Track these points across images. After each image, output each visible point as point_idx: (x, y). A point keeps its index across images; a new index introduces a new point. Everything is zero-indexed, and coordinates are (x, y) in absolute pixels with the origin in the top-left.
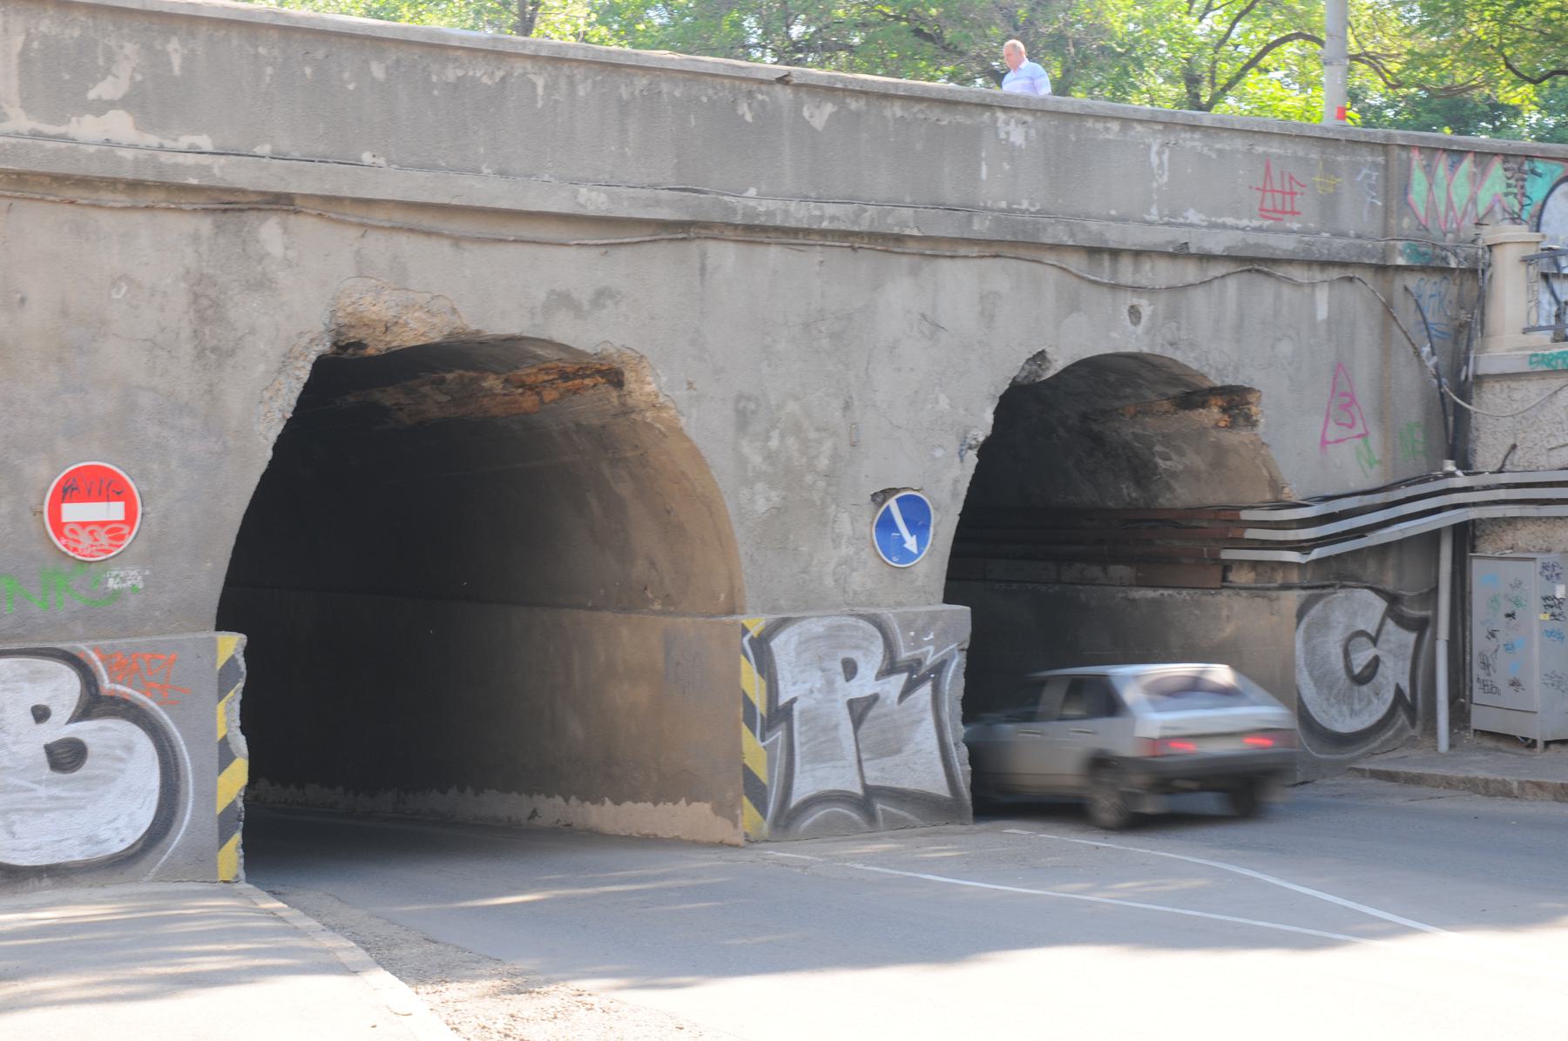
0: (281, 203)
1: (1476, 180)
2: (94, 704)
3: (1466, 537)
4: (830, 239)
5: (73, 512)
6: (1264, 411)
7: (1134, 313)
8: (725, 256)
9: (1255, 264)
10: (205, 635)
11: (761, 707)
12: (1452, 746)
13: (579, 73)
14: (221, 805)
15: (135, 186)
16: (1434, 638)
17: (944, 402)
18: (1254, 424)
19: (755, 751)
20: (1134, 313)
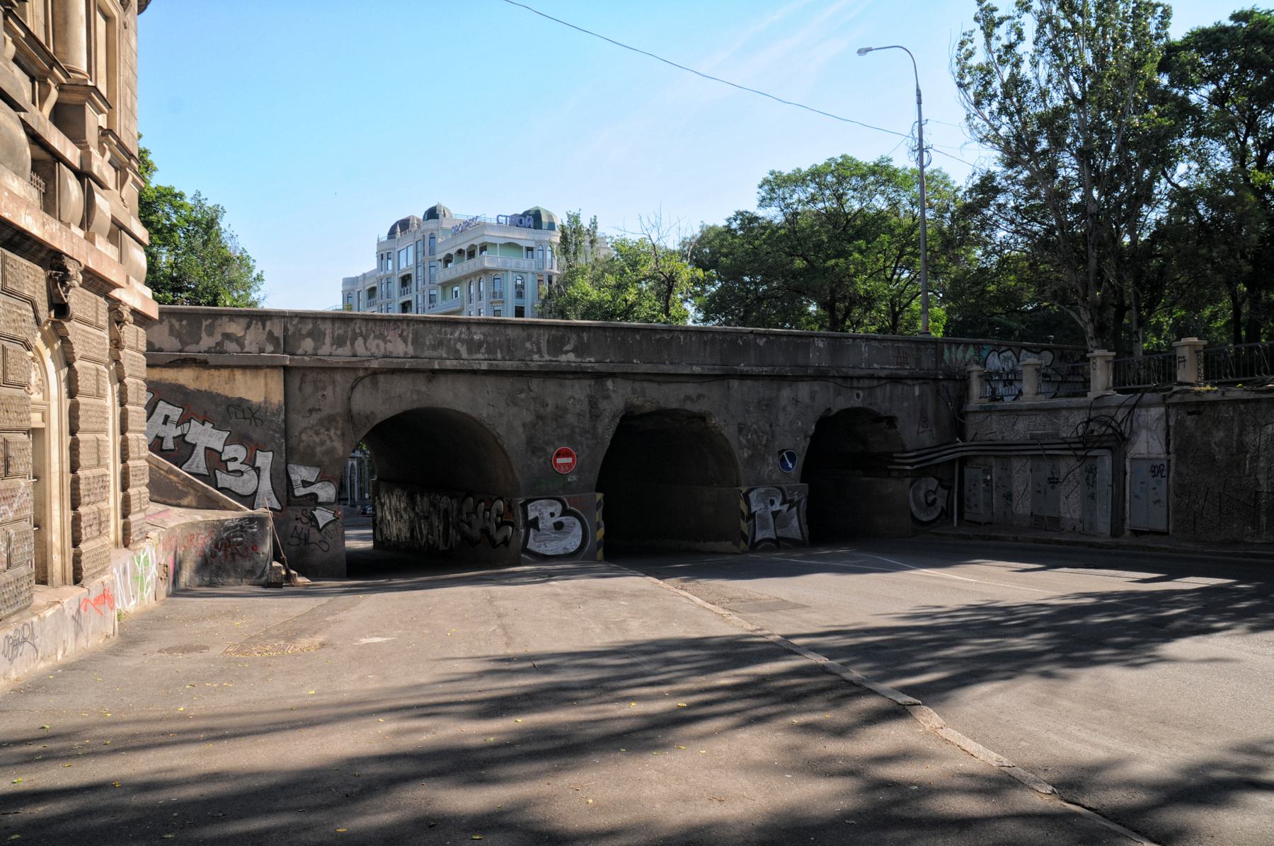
0: (612, 375)
1: (965, 352)
2: (565, 512)
3: (964, 461)
4: (108, 461)
5: (560, 461)
6: (899, 425)
7: (858, 396)
8: (735, 384)
9: (895, 379)
10: (593, 494)
11: (746, 513)
12: (958, 525)
13: (693, 334)
14: (598, 539)
15: (575, 373)
16: (954, 492)
17: (800, 423)
18: (896, 427)
19: (744, 526)
20: (858, 396)
